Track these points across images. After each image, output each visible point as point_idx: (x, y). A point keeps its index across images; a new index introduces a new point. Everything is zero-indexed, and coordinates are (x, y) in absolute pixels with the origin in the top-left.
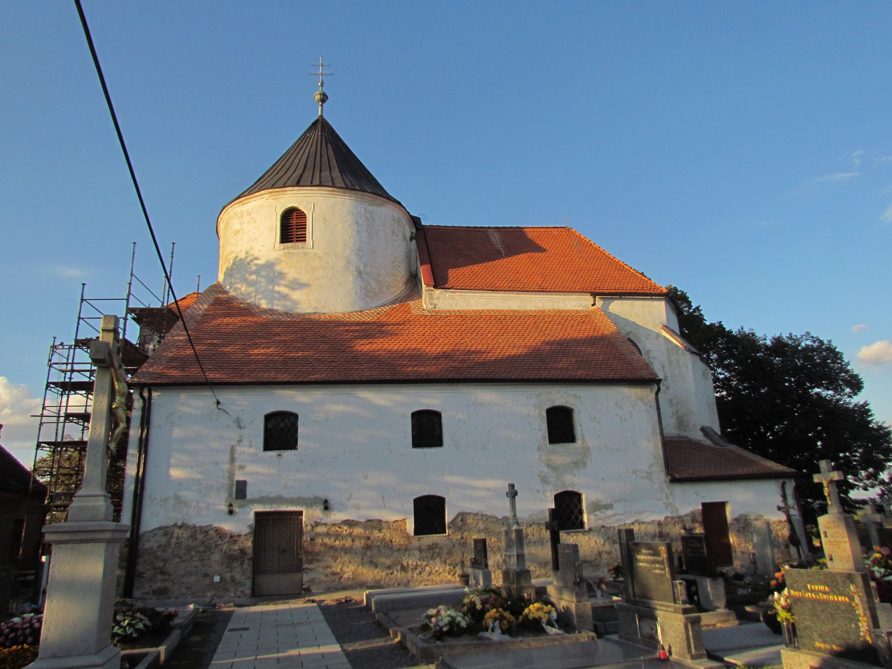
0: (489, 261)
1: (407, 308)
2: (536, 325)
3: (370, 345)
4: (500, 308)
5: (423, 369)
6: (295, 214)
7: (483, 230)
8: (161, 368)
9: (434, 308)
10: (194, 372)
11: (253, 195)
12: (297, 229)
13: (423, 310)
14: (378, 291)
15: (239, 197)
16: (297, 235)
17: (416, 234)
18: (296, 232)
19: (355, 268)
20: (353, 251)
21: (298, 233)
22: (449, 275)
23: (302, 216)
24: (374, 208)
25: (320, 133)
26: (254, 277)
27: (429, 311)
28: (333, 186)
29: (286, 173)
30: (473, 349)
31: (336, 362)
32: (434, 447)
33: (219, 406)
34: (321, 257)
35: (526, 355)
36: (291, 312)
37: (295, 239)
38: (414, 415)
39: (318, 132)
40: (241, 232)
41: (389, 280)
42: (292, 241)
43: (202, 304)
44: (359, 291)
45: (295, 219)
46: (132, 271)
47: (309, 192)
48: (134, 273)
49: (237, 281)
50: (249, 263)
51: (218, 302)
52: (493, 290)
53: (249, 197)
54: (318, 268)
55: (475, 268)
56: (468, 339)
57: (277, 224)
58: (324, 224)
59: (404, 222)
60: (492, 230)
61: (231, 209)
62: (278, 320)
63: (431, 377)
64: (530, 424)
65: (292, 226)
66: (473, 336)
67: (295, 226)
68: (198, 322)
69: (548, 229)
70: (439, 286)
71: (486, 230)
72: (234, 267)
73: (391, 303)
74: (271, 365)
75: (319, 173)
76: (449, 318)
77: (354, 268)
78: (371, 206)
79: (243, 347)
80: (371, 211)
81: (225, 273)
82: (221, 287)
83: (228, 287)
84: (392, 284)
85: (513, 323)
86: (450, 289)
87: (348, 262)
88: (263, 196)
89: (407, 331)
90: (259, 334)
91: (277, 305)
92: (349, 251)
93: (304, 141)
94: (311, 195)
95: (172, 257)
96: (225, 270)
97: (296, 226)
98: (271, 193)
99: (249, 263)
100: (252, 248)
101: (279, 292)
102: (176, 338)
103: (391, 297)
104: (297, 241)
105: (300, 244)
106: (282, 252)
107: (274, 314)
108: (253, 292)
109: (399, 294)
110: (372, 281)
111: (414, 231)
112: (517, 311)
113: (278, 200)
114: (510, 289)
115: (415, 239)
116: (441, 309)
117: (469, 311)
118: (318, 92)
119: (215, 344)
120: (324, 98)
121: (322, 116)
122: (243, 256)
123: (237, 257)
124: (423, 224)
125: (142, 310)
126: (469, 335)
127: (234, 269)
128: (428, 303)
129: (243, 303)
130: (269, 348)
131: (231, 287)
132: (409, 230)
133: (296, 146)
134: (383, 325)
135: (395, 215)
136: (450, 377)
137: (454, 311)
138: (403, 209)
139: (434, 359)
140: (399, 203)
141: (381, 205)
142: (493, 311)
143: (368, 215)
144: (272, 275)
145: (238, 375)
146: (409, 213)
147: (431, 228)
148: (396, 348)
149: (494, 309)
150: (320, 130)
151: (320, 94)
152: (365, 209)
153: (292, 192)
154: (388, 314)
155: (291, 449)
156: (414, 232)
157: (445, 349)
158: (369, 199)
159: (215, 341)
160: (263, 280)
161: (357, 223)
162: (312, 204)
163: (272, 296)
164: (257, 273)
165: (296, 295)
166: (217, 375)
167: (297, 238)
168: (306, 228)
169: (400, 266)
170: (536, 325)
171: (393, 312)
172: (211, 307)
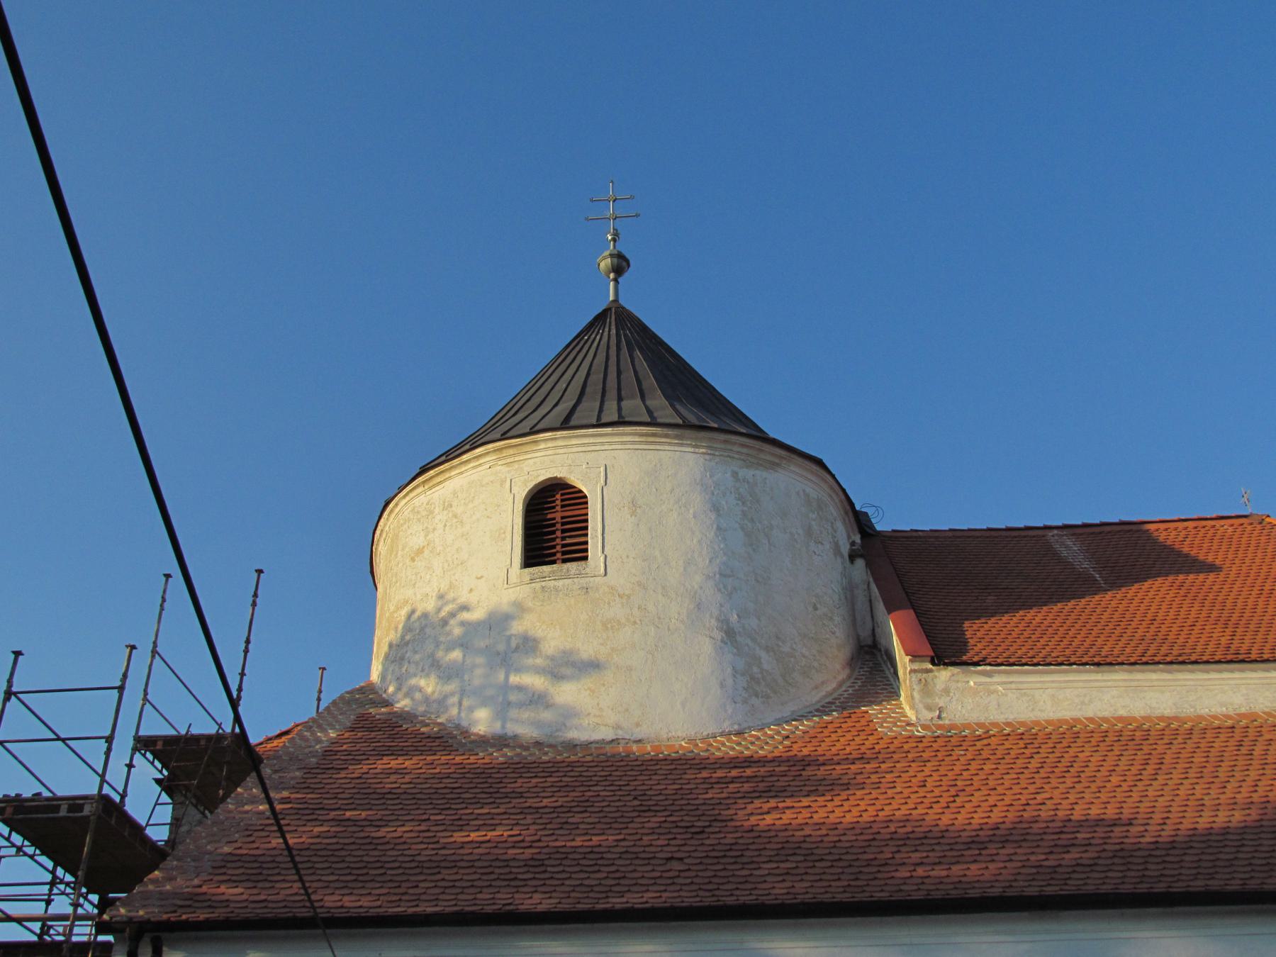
0: (1069, 600)
1: (863, 722)
2: (1244, 750)
3: (775, 815)
4: (1122, 712)
5: (944, 873)
6: (558, 496)
8: (196, 882)
9: (939, 717)
10: (283, 892)
11: (456, 462)
12: (563, 531)
13: (909, 724)
15: (424, 470)
16: (564, 546)
17: (863, 545)
18: (563, 539)
19: (718, 620)
20: (708, 577)
21: (568, 541)
22: (968, 635)
23: (577, 498)
24: (758, 472)
25: (614, 331)
26: (456, 655)
27: (925, 727)
28: (653, 423)
30: (1077, 815)
31: (681, 859)
34: (629, 597)
35: (1243, 830)
36: (552, 741)
37: (559, 555)
39: (610, 330)
40: (426, 552)
41: (807, 653)
42: (554, 562)
43: (323, 730)
44: (730, 682)
45: (558, 508)
46: (155, 643)
47: (592, 440)
49: (412, 669)
50: (445, 622)
51: (364, 723)
52: (1098, 664)
53: (446, 466)
54: (619, 622)
55: (1036, 616)
56: (1056, 792)
57: (515, 523)
58: (633, 514)
60: (1056, 532)
61: (404, 502)
62: (516, 759)
63: (973, 893)
65: (554, 525)
66: (1069, 784)
67: (559, 526)
68: (308, 770)
69: (1204, 523)
70: (947, 657)
71: (1040, 532)
72: (408, 638)
73: (817, 710)
74: (497, 871)
75: (615, 406)
76: (985, 742)
77: (714, 622)
78: (748, 467)
79: (422, 828)
81: (387, 657)
82: (376, 693)
83: (391, 689)
84: (816, 664)
85: (1174, 748)
86: (977, 664)
87: (699, 606)
88: (481, 461)
89: (874, 778)
91: (517, 721)
92: (698, 578)
93: (578, 348)
94: (598, 448)
95: (254, 604)
96: (385, 648)
97: (563, 524)
98: (500, 450)
99: (445, 622)
100: (451, 586)
101: (520, 688)
102: (247, 808)
103: (815, 698)
104: (565, 561)
105: (572, 566)
106: (527, 589)
107: (507, 746)
108: (452, 694)
109: (835, 690)
110: (763, 654)
111: (857, 539)
112: (1176, 718)
113: (516, 466)
114: (1144, 659)
115: (861, 556)
116: (959, 720)
117: (1037, 723)
118: (607, 253)
119: (348, 820)
120: (620, 266)
121: (616, 301)
122: (430, 606)
123: (413, 612)
124: (879, 528)
125: (168, 740)
126: (1054, 782)
127: (407, 644)
128: (921, 706)
129: (427, 725)
130: (493, 827)
131: (399, 689)
132: (844, 536)
134: (806, 762)
135: (808, 490)
136: (1032, 891)
137: (995, 724)
139: (970, 844)
140: (819, 463)
141: (773, 466)
142: (1105, 720)
144: (501, 647)
145: (406, 897)
147: (896, 536)
148: (849, 818)
149: (1106, 714)
150: (613, 327)
151: (612, 256)
152: (735, 474)
153: (550, 444)
154: (810, 737)
157: (996, 816)
158: (745, 450)
159: (348, 814)
160: (480, 660)
161: (716, 509)
162: (602, 469)
163: (503, 702)
164: (463, 644)
165: (568, 693)
166: (346, 898)
167: (564, 553)
168: (586, 528)
169: (831, 619)
170: (1244, 750)
171: (826, 732)
172: (347, 735)
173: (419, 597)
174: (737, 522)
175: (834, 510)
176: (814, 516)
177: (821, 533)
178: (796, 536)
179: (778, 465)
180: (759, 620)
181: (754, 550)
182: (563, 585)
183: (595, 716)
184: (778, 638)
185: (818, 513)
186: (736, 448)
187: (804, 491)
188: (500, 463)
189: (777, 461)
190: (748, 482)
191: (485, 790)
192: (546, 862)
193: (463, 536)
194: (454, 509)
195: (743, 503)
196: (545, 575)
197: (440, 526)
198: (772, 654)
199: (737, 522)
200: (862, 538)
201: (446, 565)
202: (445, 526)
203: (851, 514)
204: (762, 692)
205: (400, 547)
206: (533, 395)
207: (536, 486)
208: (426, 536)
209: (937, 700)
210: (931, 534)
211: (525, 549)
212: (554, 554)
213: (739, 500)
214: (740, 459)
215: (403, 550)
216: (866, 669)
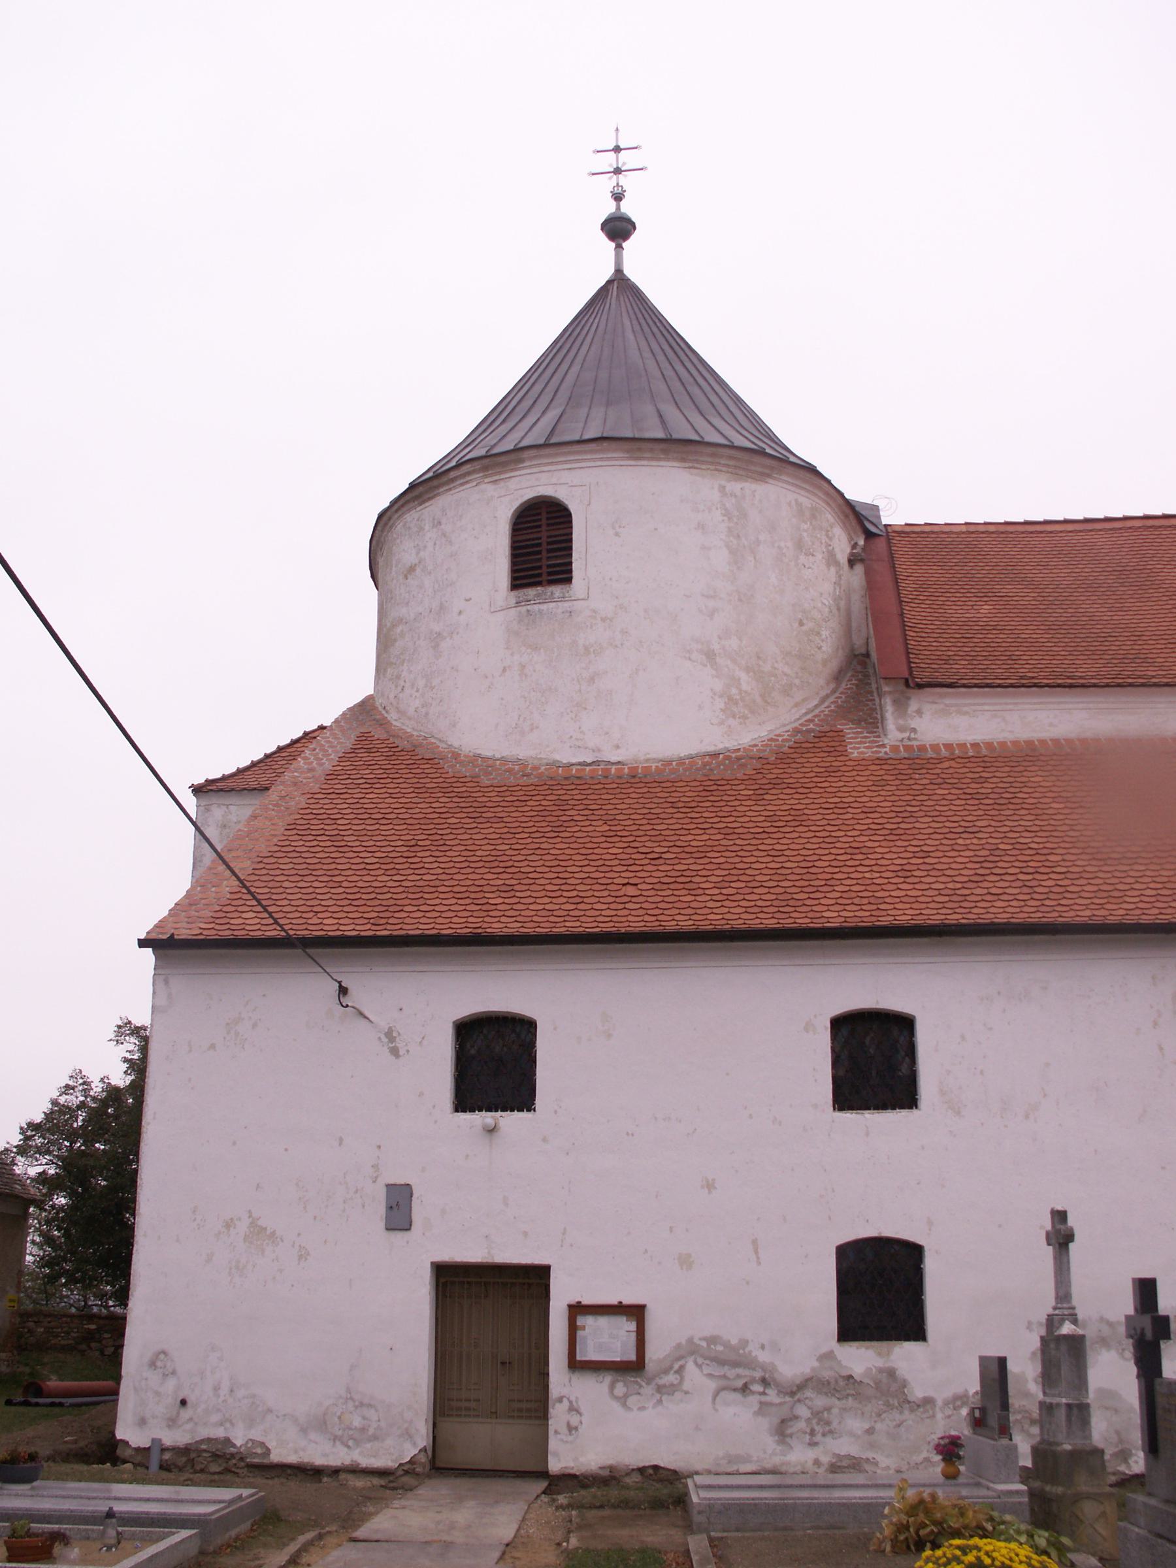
7: (1049, 528)
14: (759, 700)
17: (864, 549)
29: (524, 417)
32: (894, 1108)
33: (345, 1001)
38: (838, 1023)
40: (418, 570)
59: (829, 517)
64: (1161, 1049)
80: (738, 493)
84: (797, 681)
88: (468, 478)
90: (453, 820)
105: (557, 590)
109: (816, 706)
110: (744, 676)
113: (502, 484)
115: (862, 561)
132: (841, 542)
133: (555, 351)
138: (826, 485)
140: (812, 470)
146: (842, 495)
152: (722, 489)
155: (520, 1110)
156: (861, 542)
158: (731, 463)
167: (549, 574)
173: (412, 616)
174: (721, 539)
175: (829, 517)
176: (805, 527)
177: (813, 544)
178: (784, 551)
179: (769, 476)
180: (740, 640)
181: (738, 568)
182: (548, 609)
183: (577, 739)
184: (759, 658)
185: (811, 523)
187: (796, 500)
188: (486, 480)
189: (767, 471)
190: (736, 496)
191: (469, 815)
192: (516, 888)
193: (451, 556)
194: (443, 526)
195: (729, 519)
196: (529, 598)
198: (751, 674)
199: (721, 539)
200: (866, 539)
201: (436, 586)
202: (435, 544)
203: (852, 517)
204: (740, 712)
205: (394, 562)
206: (527, 392)
207: (522, 505)
208: (418, 553)
209: (910, 722)
210: (947, 529)
212: (540, 575)
213: (724, 515)
214: (728, 472)
215: (396, 566)
216: (854, 682)
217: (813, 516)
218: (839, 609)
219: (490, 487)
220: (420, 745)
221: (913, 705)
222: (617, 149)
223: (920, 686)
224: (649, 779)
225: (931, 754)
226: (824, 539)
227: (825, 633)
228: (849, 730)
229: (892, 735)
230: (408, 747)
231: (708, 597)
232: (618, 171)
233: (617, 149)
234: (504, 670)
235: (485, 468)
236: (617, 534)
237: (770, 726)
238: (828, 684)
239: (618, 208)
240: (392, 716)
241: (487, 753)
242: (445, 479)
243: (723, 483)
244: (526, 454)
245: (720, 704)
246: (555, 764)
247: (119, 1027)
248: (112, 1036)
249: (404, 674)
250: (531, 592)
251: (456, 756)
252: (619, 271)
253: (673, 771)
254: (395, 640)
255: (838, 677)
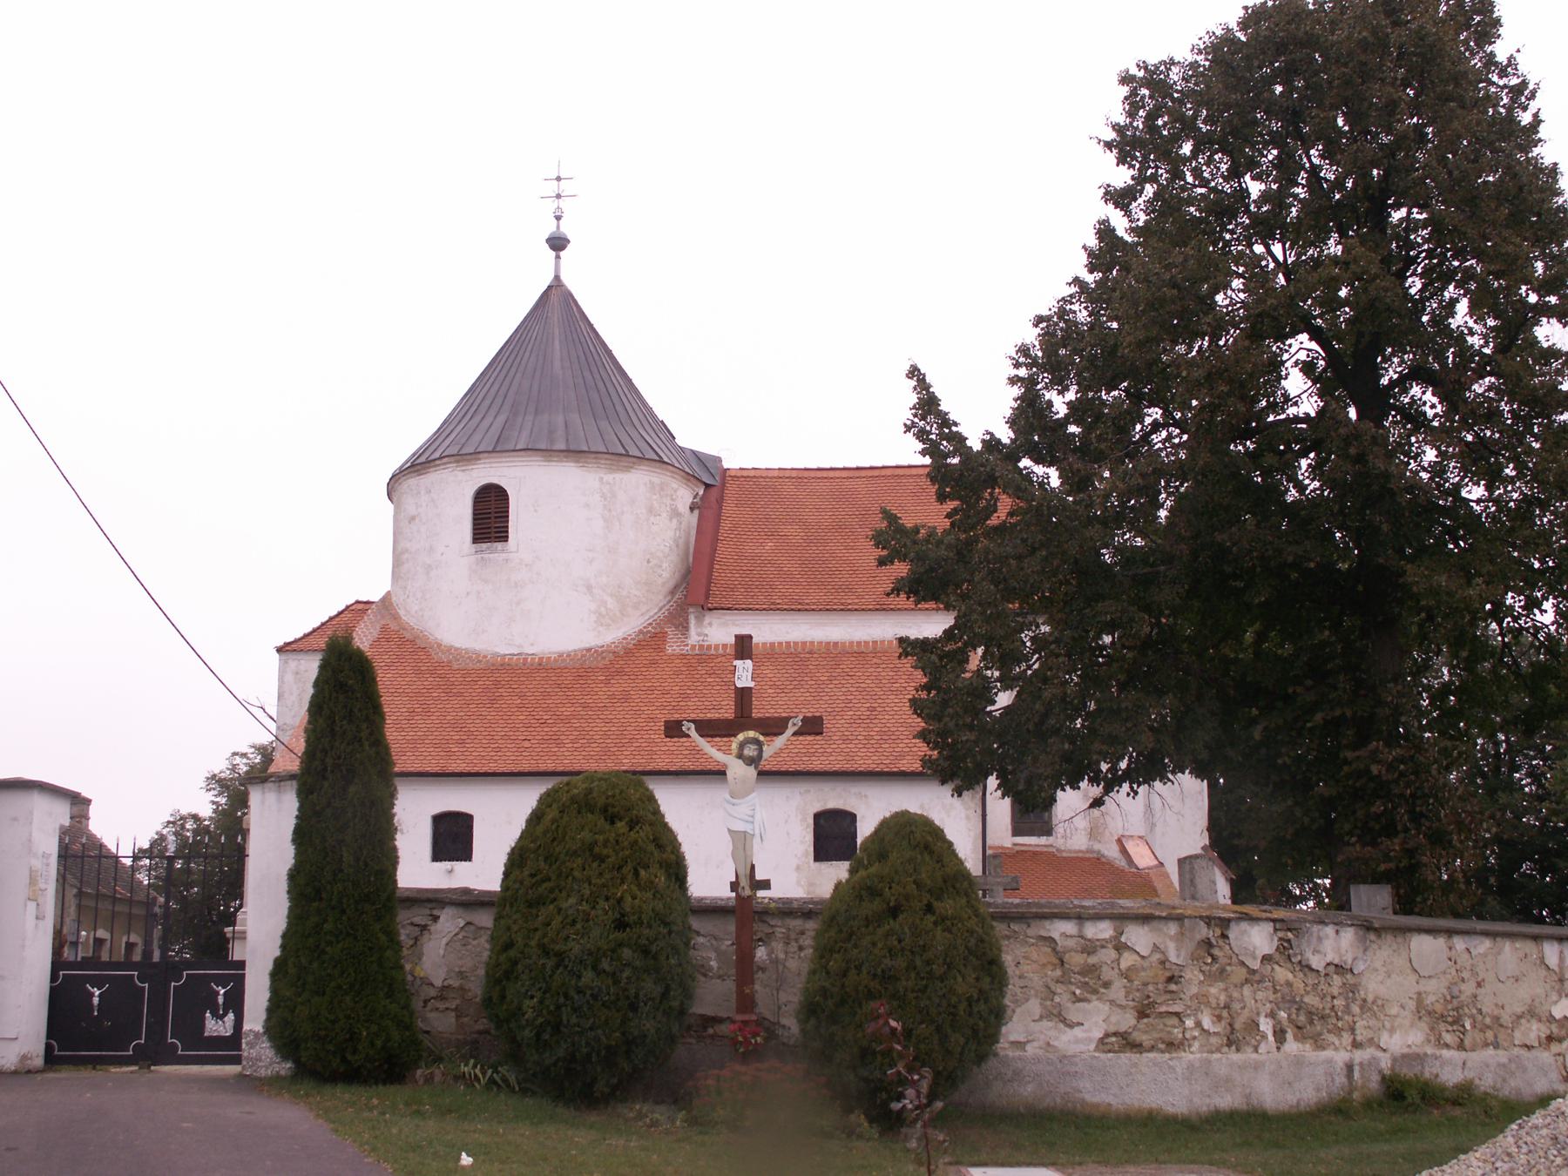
14: (618, 614)
17: (702, 499)
48: (456, 452)
84: (644, 600)
105: (499, 545)
143: (605, 491)
152: (601, 479)
158: (608, 462)
186: (603, 462)
197: (424, 504)
211: (474, 529)
217: (662, 489)
218: (677, 546)
219: (460, 474)
220: (418, 637)
221: (707, 620)
222: (559, 179)
223: (710, 609)
224: (549, 666)
225: (713, 652)
226: (668, 502)
227: (665, 565)
228: (670, 630)
229: (694, 638)
230: (411, 638)
231: (590, 550)
232: (558, 196)
233: (559, 179)
234: (468, 594)
235: (457, 462)
236: (536, 511)
237: (623, 630)
238: (665, 597)
239: (558, 227)
240: (401, 612)
241: (457, 645)
242: (432, 464)
243: (602, 475)
244: (481, 456)
245: (594, 618)
246: (496, 655)
247: (208, 778)
248: (204, 785)
249: (409, 587)
250: (484, 546)
251: (439, 645)
252: (557, 278)
253: (564, 660)
254: (403, 563)
255: (673, 592)
